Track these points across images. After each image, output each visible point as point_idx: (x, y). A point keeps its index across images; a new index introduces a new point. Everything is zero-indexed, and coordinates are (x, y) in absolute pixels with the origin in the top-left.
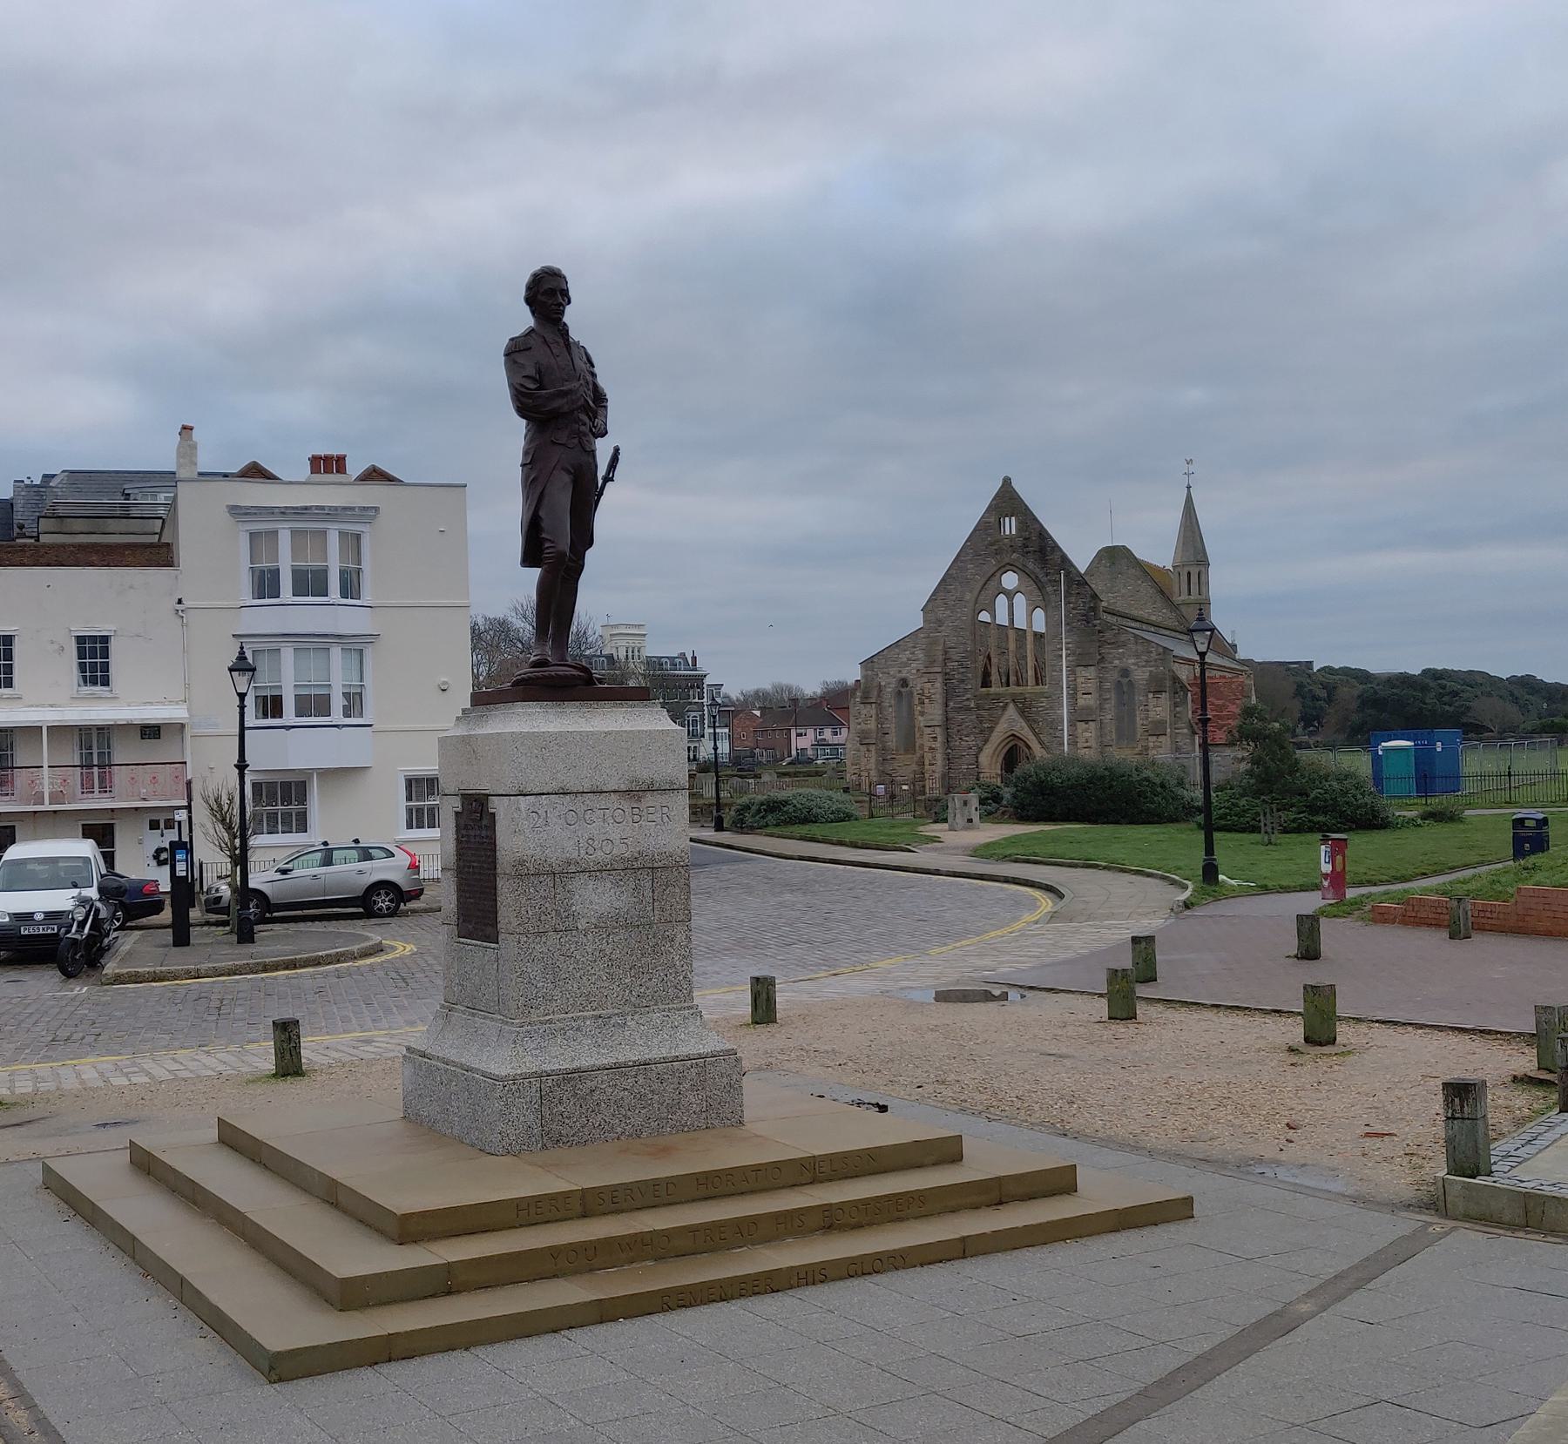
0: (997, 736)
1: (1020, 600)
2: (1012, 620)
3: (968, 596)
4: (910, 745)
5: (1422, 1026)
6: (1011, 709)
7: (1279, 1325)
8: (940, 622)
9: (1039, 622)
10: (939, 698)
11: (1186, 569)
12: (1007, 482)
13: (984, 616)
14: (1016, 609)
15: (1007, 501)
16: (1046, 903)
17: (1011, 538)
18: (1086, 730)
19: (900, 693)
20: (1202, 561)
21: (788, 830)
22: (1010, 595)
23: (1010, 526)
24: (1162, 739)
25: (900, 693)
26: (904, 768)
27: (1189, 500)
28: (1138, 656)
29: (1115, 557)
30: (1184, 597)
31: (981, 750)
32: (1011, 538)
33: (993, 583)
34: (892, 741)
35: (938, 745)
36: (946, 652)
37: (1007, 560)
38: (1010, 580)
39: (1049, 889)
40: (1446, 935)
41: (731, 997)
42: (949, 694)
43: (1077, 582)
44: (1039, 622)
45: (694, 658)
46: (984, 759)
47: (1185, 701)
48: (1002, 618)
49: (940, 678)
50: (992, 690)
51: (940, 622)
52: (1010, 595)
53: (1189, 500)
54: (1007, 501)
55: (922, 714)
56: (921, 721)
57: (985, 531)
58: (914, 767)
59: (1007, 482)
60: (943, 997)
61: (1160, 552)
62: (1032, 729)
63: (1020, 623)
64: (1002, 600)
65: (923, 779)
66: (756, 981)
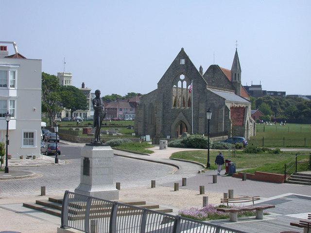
0: (177, 121)
1: (185, 83)
5: (158, 162)
7: (118, 155)
12: (182, 49)
14: (183, 84)
15: (182, 54)
17: (182, 65)
22: (182, 81)
23: (183, 62)
27: (236, 52)
29: (214, 69)
32: (182, 65)
43: (143, 215)
52: (182, 81)
53: (236, 52)
54: (182, 54)
57: (175, 64)
58: (153, 128)
59: (182, 49)
60: (292, 224)
61: (227, 65)
64: (180, 83)
65: (155, 132)
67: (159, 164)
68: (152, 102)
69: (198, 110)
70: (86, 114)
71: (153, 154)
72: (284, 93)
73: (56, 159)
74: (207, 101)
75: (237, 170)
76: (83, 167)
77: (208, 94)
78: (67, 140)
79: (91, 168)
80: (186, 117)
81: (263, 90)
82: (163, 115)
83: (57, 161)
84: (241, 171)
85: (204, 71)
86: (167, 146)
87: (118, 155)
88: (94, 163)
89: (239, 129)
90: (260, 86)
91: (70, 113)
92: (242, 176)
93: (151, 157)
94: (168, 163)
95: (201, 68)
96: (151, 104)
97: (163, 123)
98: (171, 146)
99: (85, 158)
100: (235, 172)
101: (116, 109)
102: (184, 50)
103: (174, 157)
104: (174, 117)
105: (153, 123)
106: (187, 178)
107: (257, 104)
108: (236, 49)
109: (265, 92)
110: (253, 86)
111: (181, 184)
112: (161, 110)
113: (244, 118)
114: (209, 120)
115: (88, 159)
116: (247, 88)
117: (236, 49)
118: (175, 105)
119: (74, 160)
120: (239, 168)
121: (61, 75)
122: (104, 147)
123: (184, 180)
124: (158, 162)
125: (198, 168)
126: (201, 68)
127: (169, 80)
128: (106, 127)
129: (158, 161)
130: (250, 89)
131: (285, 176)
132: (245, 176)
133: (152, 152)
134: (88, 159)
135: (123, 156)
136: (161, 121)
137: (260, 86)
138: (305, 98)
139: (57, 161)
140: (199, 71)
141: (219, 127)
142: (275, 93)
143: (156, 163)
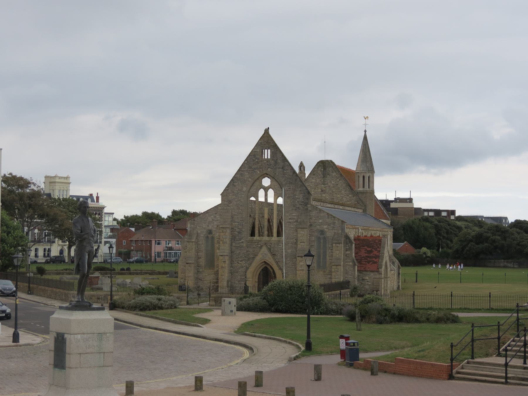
1: (271, 192)
2: (266, 199)
3: (245, 189)
4: (211, 262)
5: (216, 340)
6: (264, 249)
7: (141, 326)
8: (230, 202)
9: (280, 201)
10: (228, 241)
11: (362, 174)
12: (267, 131)
13: (253, 199)
14: (268, 195)
15: (267, 141)
16: (246, 353)
17: (265, 159)
18: (301, 261)
19: (207, 237)
20: (371, 170)
21: (148, 313)
22: (266, 189)
23: (267, 154)
24: (338, 267)
25: (207, 237)
26: (208, 277)
27: (365, 138)
28: (329, 225)
29: (325, 167)
30: (361, 189)
31: (247, 268)
32: (265, 159)
33: (257, 183)
34: (202, 261)
35: (226, 265)
36: (232, 217)
37: (265, 172)
38: (266, 182)
39: (250, 349)
40: (370, 373)
41: (211, 378)
42: (233, 238)
44: (280, 201)
45: (98, 198)
46: (249, 275)
47: (350, 249)
48: (262, 199)
49: (228, 231)
50: (255, 238)
51: (230, 202)
52: (266, 189)
54: (267, 141)
55: (219, 249)
56: (218, 252)
59: (267, 131)
61: (349, 161)
62: (275, 259)
63: (271, 200)
64: (261, 192)
65: (217, 282)
66: (127, 382)
68: (210, 227)
69: (296, 243)
70: (49, 250)
72: (453, 212)
74: (311, 225)
75: (362, 355)
77: (314, 213)
80: (274, 255)
81: (415, 207)
82: (232, 252)
83: (16, 338)
84: (371, 358)
85: (307, 173)
86: (234, 309)
87: (141, 326)
88: (73, 344)
90: (410, 200)
91: (66, 248)
92: (374, 369)
95: (302, 166)
96: (210, 232)
97: (232, 267)
98: (240, 309)
100: (357, 358)
101: (150, 241)
102: (271, 132)
104: (252, 256)
106: (263, 370)
108: (365, 131)
109: (418, 211)
110: (397, 200)
111: (251, 383)
112: (228, 242)
116: (386, 203)
117: (365, 131)
120: (366, 351)
121: (50, 180)
122: (94, 312)
123: (259, 376)
124: (216, 340)
125: (292, 352)
126: (302, 166)
128: (130, 274)
130: (393, 205)
133: (206, 321)
135: (160, 330)
136: (227, 262)
137: (410, 200)
138: (489, 222)
139: (16, 338)
140: (297, 171)
141: (333, 274)
142: (438, 212)
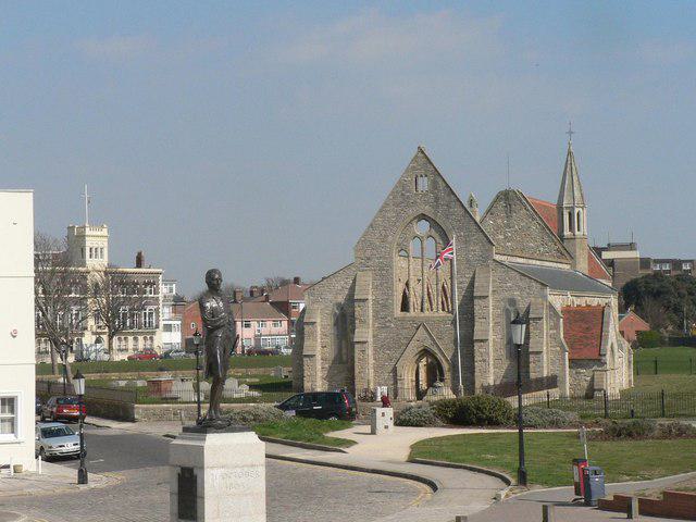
61: (542, 191)
67: (341, 470)
71: (355, 447)
73: (81, 471)
76: (176, 497)
78: (106, 417)
79: (203, 498)
83: (83, 479)
89: (60, 309)
93: (351, 455)
94: (406, 472)
99: (183, 469)
103: (419, 454)
105: (344, 358)
107: (632, 296)
113: (601, 337)
114: (519, 346)
115: (190, 470)
118: (405, 307)
119: (131, 471)
127: (386, 236)
129: (371, 468)
131: (199, 408)
132: (635, 505)
133: (350, 443)
134: (190, 470)
139: (83, 479)
143: (290, 463)
